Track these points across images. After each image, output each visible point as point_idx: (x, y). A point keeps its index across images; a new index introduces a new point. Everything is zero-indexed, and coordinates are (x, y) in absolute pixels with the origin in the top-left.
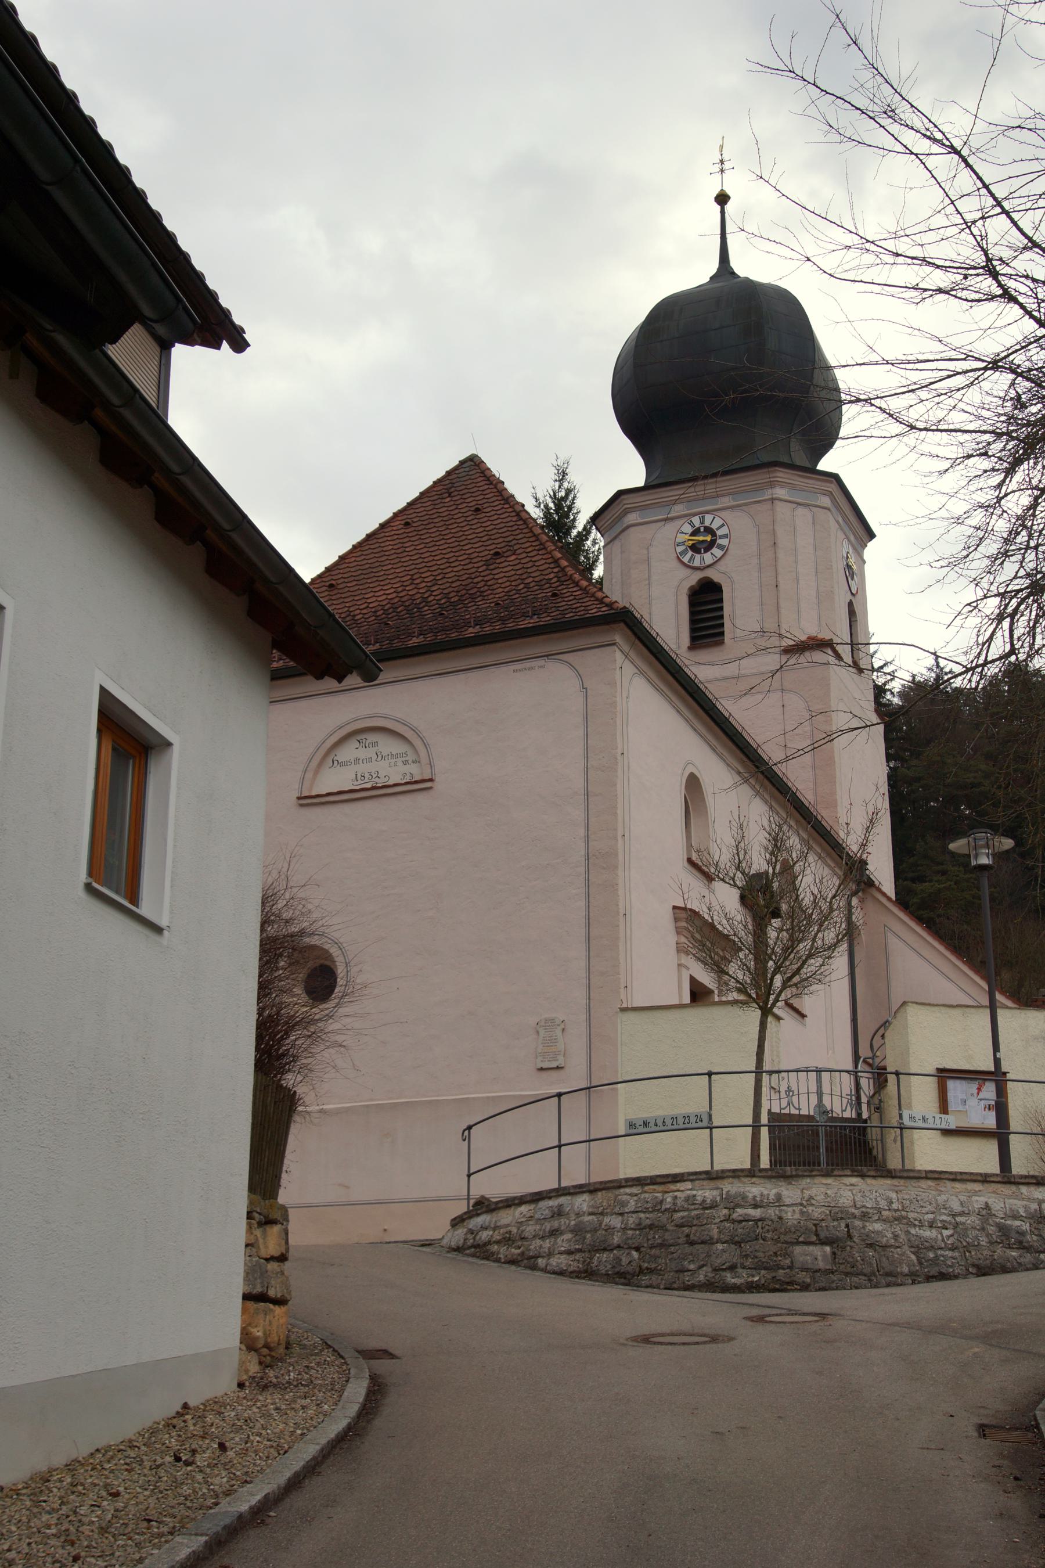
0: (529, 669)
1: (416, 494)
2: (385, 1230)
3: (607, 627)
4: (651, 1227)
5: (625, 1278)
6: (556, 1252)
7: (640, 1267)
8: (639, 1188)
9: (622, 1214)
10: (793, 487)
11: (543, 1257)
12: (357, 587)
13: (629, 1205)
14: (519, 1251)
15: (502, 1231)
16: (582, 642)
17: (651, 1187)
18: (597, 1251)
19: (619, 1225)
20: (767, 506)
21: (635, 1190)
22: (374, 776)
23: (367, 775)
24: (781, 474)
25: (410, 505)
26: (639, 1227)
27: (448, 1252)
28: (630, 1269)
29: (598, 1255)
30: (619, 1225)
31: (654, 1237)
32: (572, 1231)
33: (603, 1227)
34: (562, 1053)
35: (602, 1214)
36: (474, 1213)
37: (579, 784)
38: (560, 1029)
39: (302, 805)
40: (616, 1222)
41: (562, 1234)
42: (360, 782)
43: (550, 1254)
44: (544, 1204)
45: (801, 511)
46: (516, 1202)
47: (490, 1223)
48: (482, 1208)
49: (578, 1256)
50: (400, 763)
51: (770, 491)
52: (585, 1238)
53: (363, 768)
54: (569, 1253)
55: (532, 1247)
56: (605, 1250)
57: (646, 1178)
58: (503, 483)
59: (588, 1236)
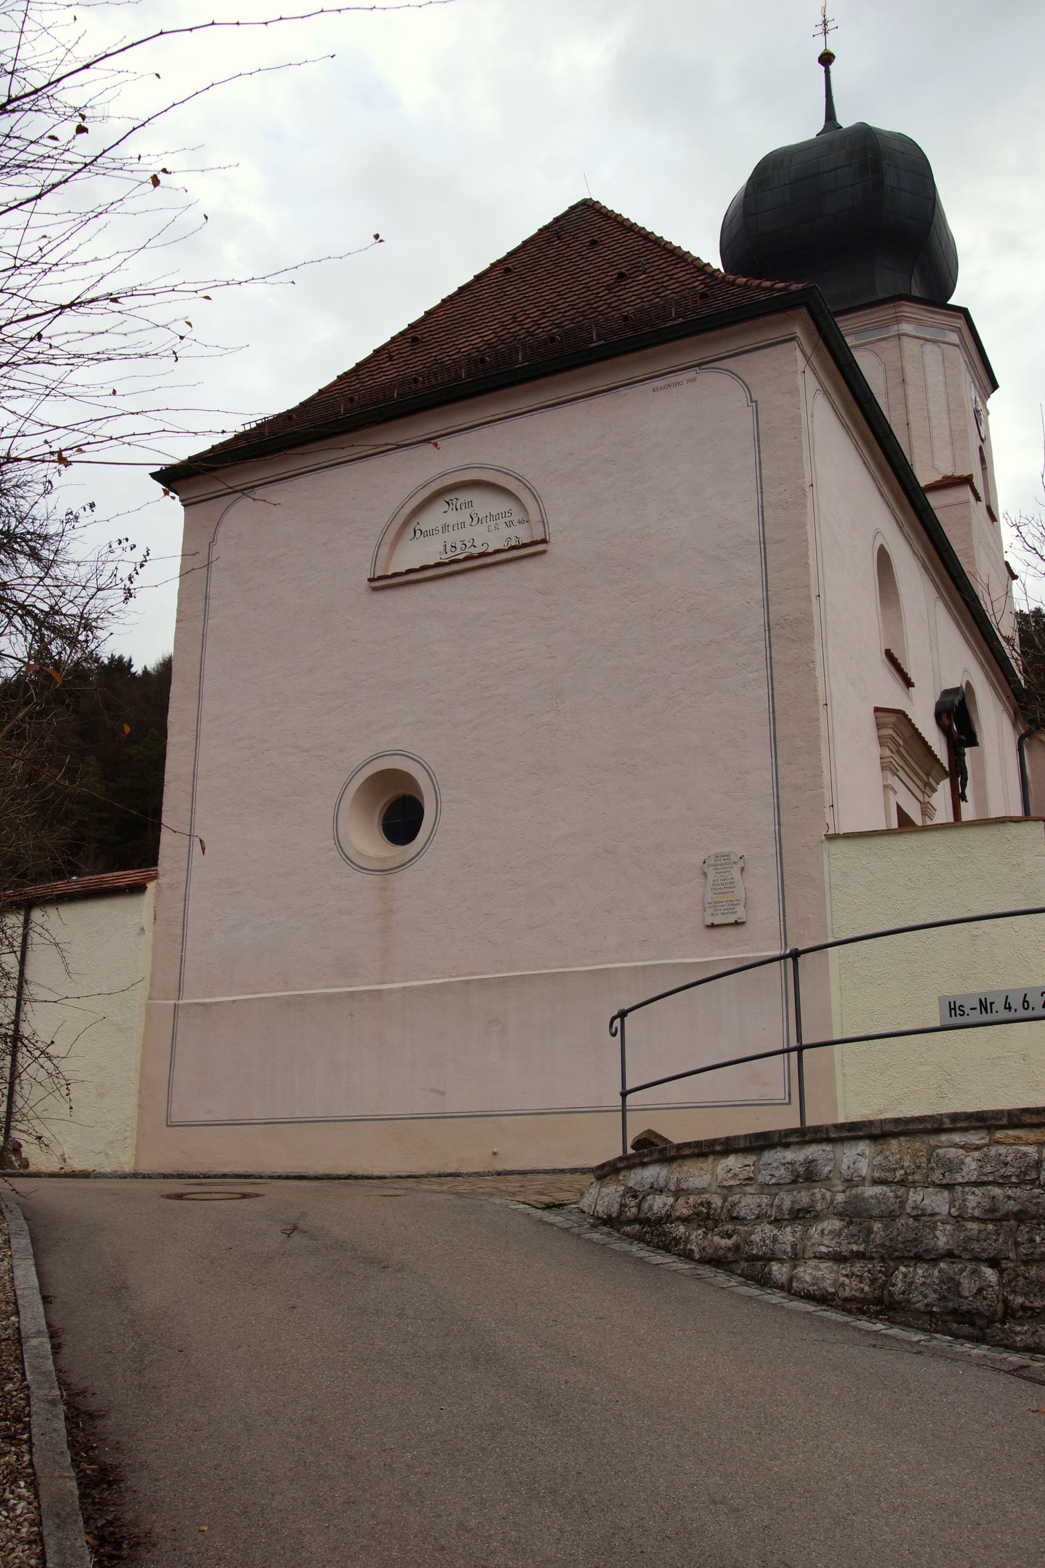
0: (674, 385)
1: (518, 243)
2: (495, 1154)
3: (783, 315)
4: (1020, 1216)
5: (972, 1324)
6: (809, 1254)
7: (1005, 1301)
8: (983, 1133)
9: (949, 1187)
10: (919, 323)
11: (781, 1261)
12: (446, 337)
13: (965, 1169)
14: (729, 1242)
15: (691, 1199)
16: (748, 342)
17: (1010, 1132)
18: (901, 1260)
19: (944, 1209)
20: (894, 342)
21: (974, 1138)
22: (468, 545)
23: (459, 545)
24: (908, 309)
25: (510, 255)
26: (992, 1215)
27: (594, 1226)
28: (981, 1305)
29: (903, 1269)
30: (944, 1209)
31: (1032, 1240)
32: (840, 1215)
33: (909, 1210)
34: (742, 903)
35: (902, 1183)
36: (637, 1160)
37: (752, 528)
38: (736, 868)
39: (375, 589)
40: (938, 1202)
41: (818, 1217)
42: (450, 554)
43: (796, 1258)
44: (774, 1157)
45: (929, 347)
46: (718, 1148)
47: (667, 1182)
48: (651, 1153)
49: (857, 1268)
50: (502, 526)
51: (895, 327)
52: (870, 1231)
53: (453, 537)
54: (838, 1258)
55: (756, 1238)
56: (918, 1258)
57: (999, 1114)
58: (620, 215)
59: (877, 1226)
